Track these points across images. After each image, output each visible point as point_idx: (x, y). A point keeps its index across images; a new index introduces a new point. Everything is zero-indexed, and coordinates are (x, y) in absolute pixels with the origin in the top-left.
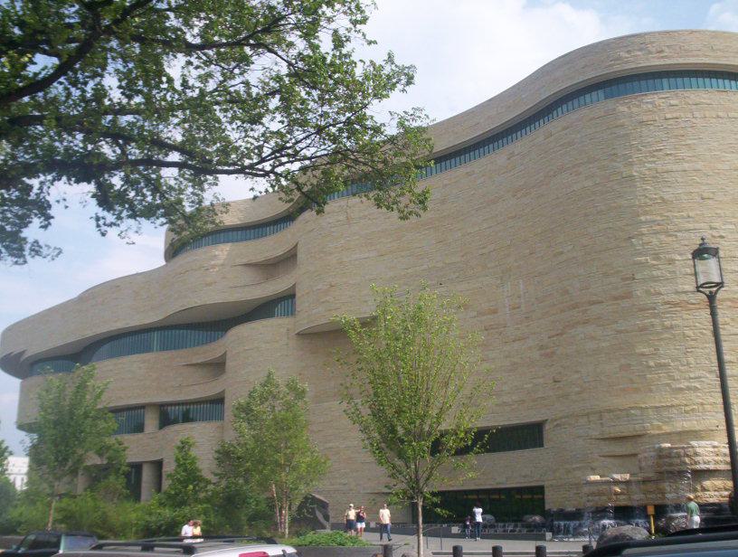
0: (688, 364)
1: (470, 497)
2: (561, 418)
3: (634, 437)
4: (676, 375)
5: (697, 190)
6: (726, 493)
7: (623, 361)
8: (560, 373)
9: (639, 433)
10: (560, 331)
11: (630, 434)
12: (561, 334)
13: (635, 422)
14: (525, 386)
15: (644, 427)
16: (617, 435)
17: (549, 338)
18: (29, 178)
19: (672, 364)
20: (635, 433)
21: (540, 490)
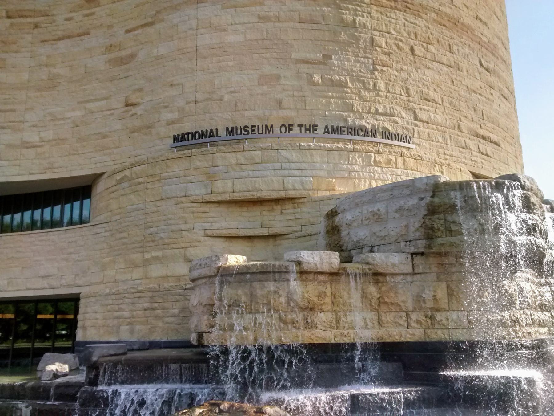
0: (375, 89)
1: (28, 345)
2: (133, 165)
3: (277, 201)
4: (357, 105)
5: (435, 52)
6: (448, 338)
7: (267, 70)
8: (140, 90)
9: (292, 194)
10: (150, 20)
11: (275, 195)
12: (151, 24)
13: (286, 172)
14: (69, 115)
15: (302, 183)
16: (249, 196)
17: (128, 31)
18: (443, 371)
19: (350, 85)
20: (283, 194)
21: (75, 300)
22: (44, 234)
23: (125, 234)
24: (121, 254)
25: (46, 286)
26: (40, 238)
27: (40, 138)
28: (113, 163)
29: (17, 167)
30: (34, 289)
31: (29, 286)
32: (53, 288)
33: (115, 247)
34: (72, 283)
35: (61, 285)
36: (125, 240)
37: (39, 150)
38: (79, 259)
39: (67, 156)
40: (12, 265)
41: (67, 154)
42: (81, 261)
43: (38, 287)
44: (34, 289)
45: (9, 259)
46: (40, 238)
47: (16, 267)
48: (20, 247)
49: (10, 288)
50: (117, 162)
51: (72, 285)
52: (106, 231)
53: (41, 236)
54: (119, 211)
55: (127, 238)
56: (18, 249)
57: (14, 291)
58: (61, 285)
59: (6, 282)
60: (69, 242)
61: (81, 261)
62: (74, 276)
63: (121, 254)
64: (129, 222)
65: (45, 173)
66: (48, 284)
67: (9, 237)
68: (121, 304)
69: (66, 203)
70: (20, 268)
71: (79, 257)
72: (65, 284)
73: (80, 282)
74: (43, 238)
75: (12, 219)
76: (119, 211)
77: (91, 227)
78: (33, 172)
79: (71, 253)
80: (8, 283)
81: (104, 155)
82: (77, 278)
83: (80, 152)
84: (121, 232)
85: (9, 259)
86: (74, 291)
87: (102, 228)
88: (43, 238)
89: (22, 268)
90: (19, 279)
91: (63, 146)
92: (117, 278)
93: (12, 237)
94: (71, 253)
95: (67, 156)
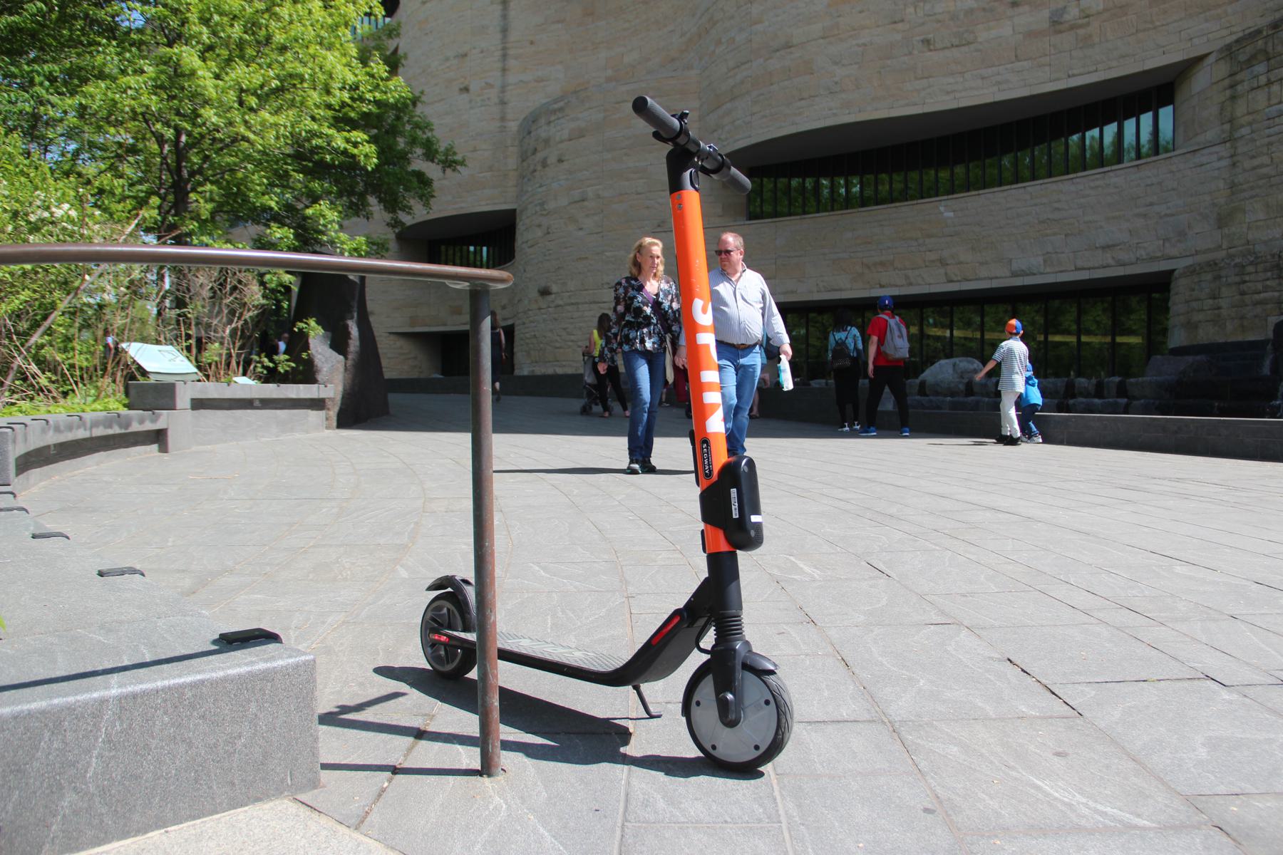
3: (303, 803)
22: (1098, 176)
23: (1266, 160)
24: (1257, 196)
25: (1111, 262)
26: (1092, 184)
27: (1082, 11)
28: (1225, 32)
29: (1047, 68)
30: (1089, 269)
31: (1080, 263)
32: (1124, 265)
33: (1241, 184)
34: (1159, 254)
35: (1137, 259)
36: (1264, 171)
37: (1081, 32)
38: (1168, 212)
39: (1133, 34)
40: (1048, 232)
41: (949, 45)
42: (1172, 215)
43: (1096, 265)
44: (1089, 269)
45: (1043, 222)
46: (1092, 184)
47: (1055, 234)
48: (1059, 201)
49: (1048, 270)
50: (1234, 29)
51: (1158, 257)
52: (1220, 159)
53: (1093, 180)
54: (1249, 118)
55: (1268, 166)
56: (1056, 205)
57: (1056, 273)
58: (1137, 259)
59: (1041, 259)
60: (1147, 185)
61: (1172, 215)
62: (1161, 242)
63: (1257, 196)
64: (1269, 136)
65: (1096, 71)
66: (1113, 258)
67: (1038, 187)
68: (1268, 279)
69: (1127, 118)
70: (1063, 236)
71: (1168, 208)
72: (1145, 257)
73: (1174, 252)
74: (1098, 183)
75: (1120, 134)
76: (1249, 118)
77: (1188, 156)
78: (1075, 72)
79: (1151, 204)
80: (1045, 261)
81: (1207, 21)
82: (1167, 245)
83: (1158, 23)
84: (1253, 157)
85: (1043, 222)
86: (1163, 266)
87: (1211, 154)
88: (1098, 183)
89: (1066, 236)
90: (1063, 253)
91: (1124, 19)
92: (1250, 237)
93: (1043, 186)
94: (1151, 204)
95: (1133, 34)
